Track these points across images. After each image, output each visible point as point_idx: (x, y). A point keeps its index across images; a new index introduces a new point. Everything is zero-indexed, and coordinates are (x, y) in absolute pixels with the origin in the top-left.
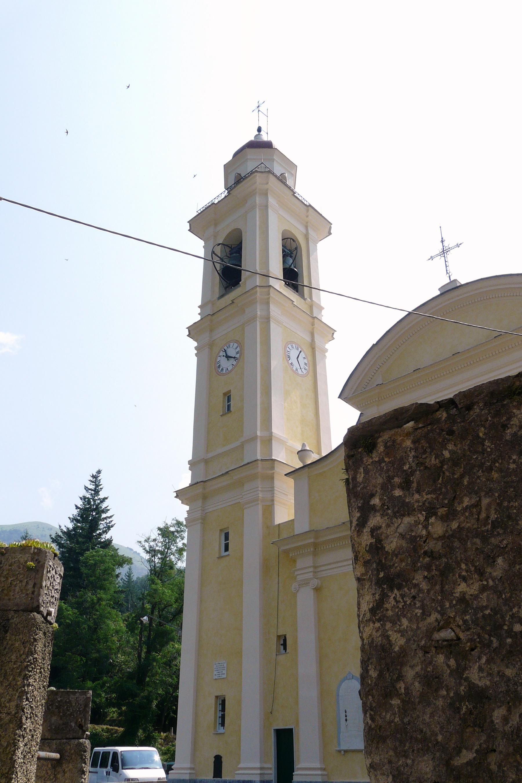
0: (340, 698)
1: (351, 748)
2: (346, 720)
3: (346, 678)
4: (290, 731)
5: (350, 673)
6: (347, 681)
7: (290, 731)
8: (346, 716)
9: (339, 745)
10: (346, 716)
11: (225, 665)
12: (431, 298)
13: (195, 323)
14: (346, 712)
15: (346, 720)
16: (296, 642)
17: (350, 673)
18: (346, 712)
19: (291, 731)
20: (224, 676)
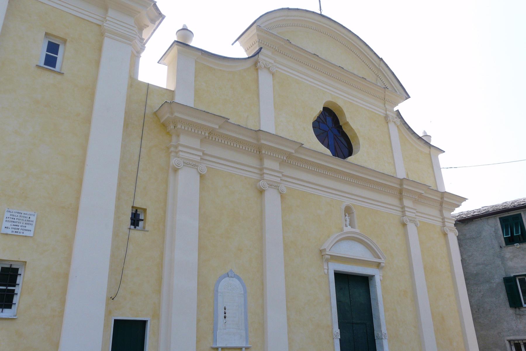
0: (219, 294)
1: (450, 242)
2: (225, 317)
3: (223, 277)
4: (140, 326)
5: (231, 271)
6: (227, 279)
7: (140, 326)
8: (225, 313)
9: (215, 340)
10: (225, 313)
11: (33, 218)
12: (387, 63)
13: (288, 9)
14: (225, 309)
15: (225, 317)
16: (117, 218)
17: (231, 271)
18: (225, 309)
19: (144, 323)
20: (31, 234)
